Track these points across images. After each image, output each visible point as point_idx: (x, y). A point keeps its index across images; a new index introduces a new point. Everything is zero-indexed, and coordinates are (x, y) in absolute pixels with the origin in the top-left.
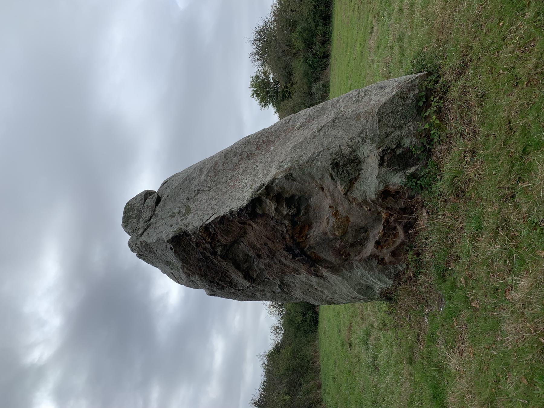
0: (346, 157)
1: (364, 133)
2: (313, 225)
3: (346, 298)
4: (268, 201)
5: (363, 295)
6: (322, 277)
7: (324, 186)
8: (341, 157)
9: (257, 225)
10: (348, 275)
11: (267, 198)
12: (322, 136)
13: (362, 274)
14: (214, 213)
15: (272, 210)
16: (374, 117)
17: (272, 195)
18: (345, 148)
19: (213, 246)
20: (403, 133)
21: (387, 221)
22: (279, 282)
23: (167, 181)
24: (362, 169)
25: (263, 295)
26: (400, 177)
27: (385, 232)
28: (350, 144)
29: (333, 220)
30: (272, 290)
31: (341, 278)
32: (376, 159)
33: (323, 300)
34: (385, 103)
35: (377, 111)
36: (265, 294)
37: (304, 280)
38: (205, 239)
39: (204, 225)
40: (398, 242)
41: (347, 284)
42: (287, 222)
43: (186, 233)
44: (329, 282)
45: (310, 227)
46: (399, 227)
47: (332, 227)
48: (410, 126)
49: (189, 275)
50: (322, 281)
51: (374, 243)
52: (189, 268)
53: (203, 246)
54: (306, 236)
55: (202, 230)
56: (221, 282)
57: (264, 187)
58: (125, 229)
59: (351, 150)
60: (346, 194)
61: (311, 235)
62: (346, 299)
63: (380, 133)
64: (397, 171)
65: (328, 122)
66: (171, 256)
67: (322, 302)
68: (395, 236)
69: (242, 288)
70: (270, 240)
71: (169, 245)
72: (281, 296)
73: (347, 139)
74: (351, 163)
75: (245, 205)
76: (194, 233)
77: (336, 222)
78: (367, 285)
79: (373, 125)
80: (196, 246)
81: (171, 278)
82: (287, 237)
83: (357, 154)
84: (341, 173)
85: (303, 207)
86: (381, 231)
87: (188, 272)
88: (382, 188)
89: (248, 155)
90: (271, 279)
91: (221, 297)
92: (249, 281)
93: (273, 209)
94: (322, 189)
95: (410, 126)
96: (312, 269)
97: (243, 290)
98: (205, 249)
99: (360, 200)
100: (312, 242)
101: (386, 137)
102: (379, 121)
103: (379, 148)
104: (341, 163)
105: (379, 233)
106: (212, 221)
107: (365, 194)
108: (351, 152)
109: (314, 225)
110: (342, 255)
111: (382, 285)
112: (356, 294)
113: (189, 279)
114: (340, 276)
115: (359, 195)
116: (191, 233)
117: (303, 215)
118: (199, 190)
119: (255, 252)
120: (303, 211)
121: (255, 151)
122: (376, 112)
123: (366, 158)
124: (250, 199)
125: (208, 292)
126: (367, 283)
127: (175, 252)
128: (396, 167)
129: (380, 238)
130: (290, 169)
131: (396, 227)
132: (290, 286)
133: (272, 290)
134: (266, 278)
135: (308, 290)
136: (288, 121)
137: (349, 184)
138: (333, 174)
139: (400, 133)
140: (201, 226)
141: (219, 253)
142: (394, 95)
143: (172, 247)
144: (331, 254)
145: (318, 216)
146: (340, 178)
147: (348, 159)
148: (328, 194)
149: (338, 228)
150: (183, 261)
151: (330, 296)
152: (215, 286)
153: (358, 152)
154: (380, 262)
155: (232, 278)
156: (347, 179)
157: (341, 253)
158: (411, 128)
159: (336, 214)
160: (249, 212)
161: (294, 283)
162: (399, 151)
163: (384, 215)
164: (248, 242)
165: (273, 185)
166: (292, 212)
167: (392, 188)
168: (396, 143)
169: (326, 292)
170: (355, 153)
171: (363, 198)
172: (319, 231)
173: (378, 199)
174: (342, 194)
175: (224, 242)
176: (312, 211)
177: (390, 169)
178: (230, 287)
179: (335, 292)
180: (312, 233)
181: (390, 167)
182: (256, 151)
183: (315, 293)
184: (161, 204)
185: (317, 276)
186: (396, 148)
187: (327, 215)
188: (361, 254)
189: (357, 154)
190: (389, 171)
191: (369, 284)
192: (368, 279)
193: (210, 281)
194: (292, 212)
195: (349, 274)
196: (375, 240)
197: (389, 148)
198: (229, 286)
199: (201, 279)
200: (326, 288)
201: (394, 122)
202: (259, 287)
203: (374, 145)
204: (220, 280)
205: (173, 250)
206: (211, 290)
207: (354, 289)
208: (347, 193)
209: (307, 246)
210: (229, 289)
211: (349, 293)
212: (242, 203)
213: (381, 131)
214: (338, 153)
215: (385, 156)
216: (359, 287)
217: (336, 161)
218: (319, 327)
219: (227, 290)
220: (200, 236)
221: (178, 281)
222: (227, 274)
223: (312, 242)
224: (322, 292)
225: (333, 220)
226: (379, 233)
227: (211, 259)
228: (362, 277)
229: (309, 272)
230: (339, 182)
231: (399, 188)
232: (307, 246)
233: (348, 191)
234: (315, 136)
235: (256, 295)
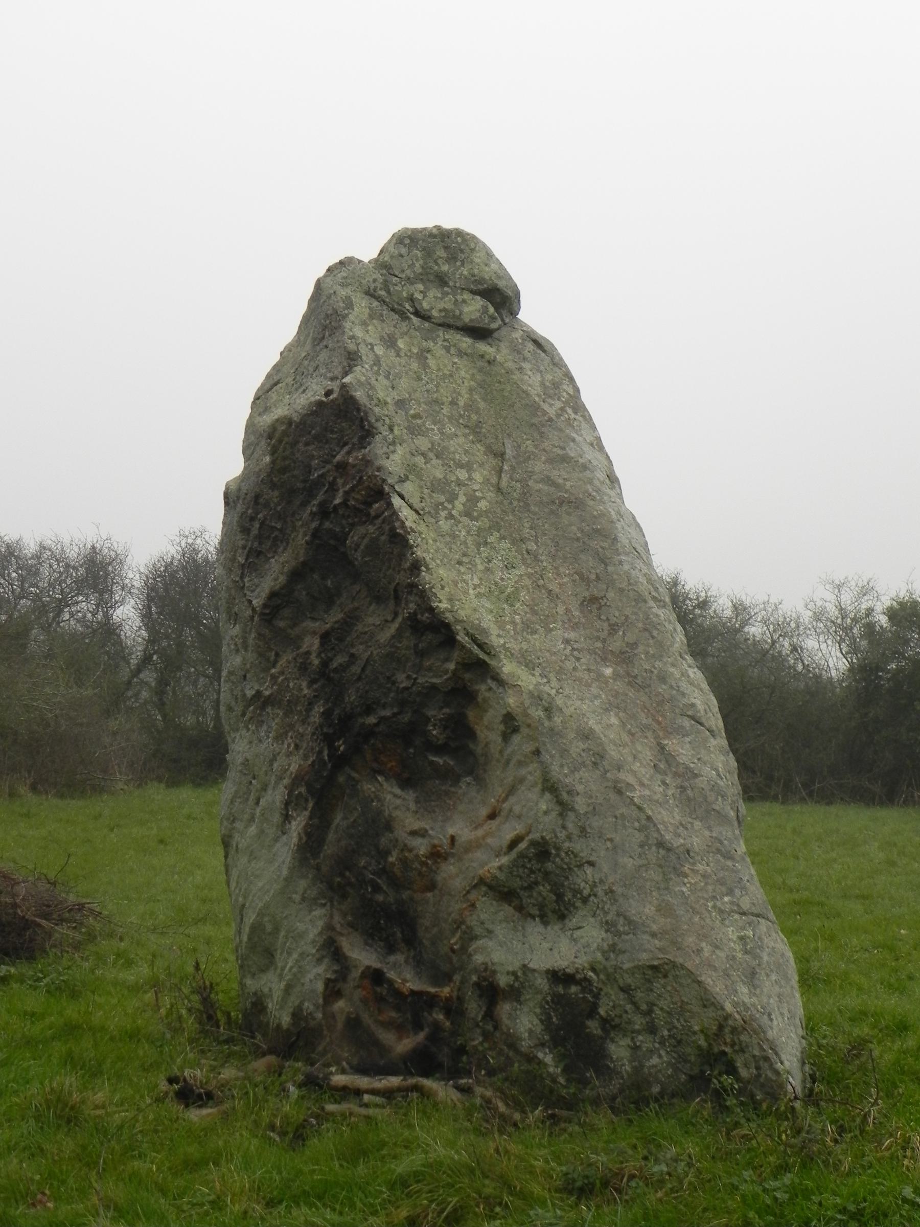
0: (567, 878)
1: (626, 928)
2: (411, 792)
3: (240, 890)
4: (452, 666)
5: (250, 939)
6: (287, 818)
7: (498, 820)
8: (565, 867)
9: (393, 637)
10: (296, 893)
11: (457, 663)
12: (620, 811)
13: (301, 935)
14: (421, 512)
15: (432, 677)
16: (663, 953)
17: (467, 676)
18: (590, 877)
19: (341, 512)
20: (640, 1038)
21: (431, 1001)
22: (267, 693)
23: (544, 351)
24: (545, 923)
25: (236, 645)
26: (530, 1032)
27: (406, 997)
28: (600, 891)
29: (421, 846)
30: (248, 671)
31: (285, 872)
32: (566, 963)
33: (233, 821)
34: (699, 983)
35: (680, 960)
36: (237, 651)
37: (275, 765)
38: (354, 491)
39: (387, 488)
40: (387, 1037)
41: (272, 891)
42: (406, 718)
43: (367, 436)
44: (276, 840)
45: (406, 783)
46: (421, 1036)
47: (405, 845)
48: (660, 1057)
49: (270, 437)
50: (277, 818)
51: (377, 965)
52: (286, 439)
53: (340, 481)
54: (380, 772)
55: (374, 481)
56: (258, 526)
57: (482, 655)
58: (394, 241)
59: (586, 892)
60: (482, 881)
61: (385, 785)
62: (237, 891)
63: (626, 971)
64: (546, 1022)
65: (658, 830)
66: (315, 391)
67: (228, 819)
68: (400, 1029)
69: (247, 585)
70: (363, 670)
71: (335, 386)
72: (237, 698)
73: (611, 879)
74: (556, 894)
75: (434, 605)
76: (367, 462)
77: (417, 856)
78: (276, 950)
79: (645, 951)
80: (338, 463)
81: (269, 376)
82: (372, 720)
83: (576, 908)
84: (529, 866)
85: (452, 763)
86: (408, 985)
87: (277, 435)
88: (503, 981)
89: (597, 599)
90: (273, 671)
91: (224, 523)
92: (265, 606)
93: (434, 680)
94: (492, 816)
95: (660, 1057)
96: (303, 790)
97: (243, 588)
98: (333, 488)
99: (472, 921)
100: (368, 788)
101: (622, 989)
102: (654, 968)
103: (593, 969)
104: (549, 866)
105: (405, 981)
106: (395, 513)
107: (485, 936)
108: (580, 892)
109: (410, 796)
110: (342, 875)
111: (277, 994)
112: (250, 918)
113: (261, 435)
114: (291, 870)
115: (483, 916)
116: (367, 450)
117: (432, 763)
118: (501, 455)
119: (336, 626)
120: (441, 761)
121: (608, 619)
122: (676, 960)
123: (572, 935)
124: (449, 617)
125: (233, 487)
126: (279, 951)
127: (320, 404)
128: (555, 1019)
129: (391, 982)
130: (529, 726)
131: (422, 1029)
132: (261, 726)
133: (248, 671)
134: (277, 655)
135: (254, 778)
136: (690, 713)
137: (506, 890)
138: (523, 846)
139: (637, 1027)
140: (384, 481)
141: (327, 525)
142: (723, 1009)
143: (331, 397)
144: (343, 843)
145: (433, 803)
146: (514, 864)
147: (563, 885)
148: (480, 832)
149: (404, 862)
150: (300, 423)
151: (243, 844)
152: (247, 509)
153: (585, 913)
154: (331, 985)
155: (270, 558)
156: (517, 883)
157: (347, 874)
158: (655, 1060)
159: (436, 855)
160: (419, 616)
161: (268, 737)
162: (593, 1026)
163: (446, 991)
164: (358, 608)
165: (489, 681)
166: (434, 732)
167: (505, 1008)
168: (610, 1015)
169: (253, 830)
170: (579, 904)
171: (478, 931)
172: (396, 808)
173: (476, 970)
174: (481, 872)
175: (353, 538)
176: (443, 788)
177: (547, 1003)
178: (249, 552)
179: (252, 857)
180: (389, 789)
181: (552, 1000)
182: (606, 625)
183: (247, 799)
184: (466, 342)
185: (287, 804)
186: (601, 1017)
187: (432, 829)
188: (351, 930)
189: (576, 908)
190: (544, 998)
191: (278, 956)
192: (289, 954)
193: (257, 497)
194: (434, 732)
195: (297, 897)
196: (385, 970)
197: (597, 996)
198: (251, 548)
199: (260, 470)
200: (262, 832)
201: (662, 1009)
202: (253, 635)
203: (599, 955)
204: (262, 524)
205: (324, 399)
206: (238, 498)
207: (261, 914)
208: (486, 884)
209: (355, 775)
210: (244, 547)
211: (251, 898)
212: (441, 595)
213: (633, 974)
214: (572, 856)
215: (579, 988)
216: (269, 927)
217: (553, 851)
218: (833, 809)
219: (241, 543)
220: (361, 478)
221: (258, 399)
222: (279, 543)
223: (368, 788)
224: (252, 819)
225: (421, 846)
226: (405, 981)
227: (310, 502)
228: (291, 934)
229: (297, 780)
230: (505, 860)
231: (505, 1031)
232: (355, 775)
233: (490, 887)
234: (619, 792)
235: (235, 624)
